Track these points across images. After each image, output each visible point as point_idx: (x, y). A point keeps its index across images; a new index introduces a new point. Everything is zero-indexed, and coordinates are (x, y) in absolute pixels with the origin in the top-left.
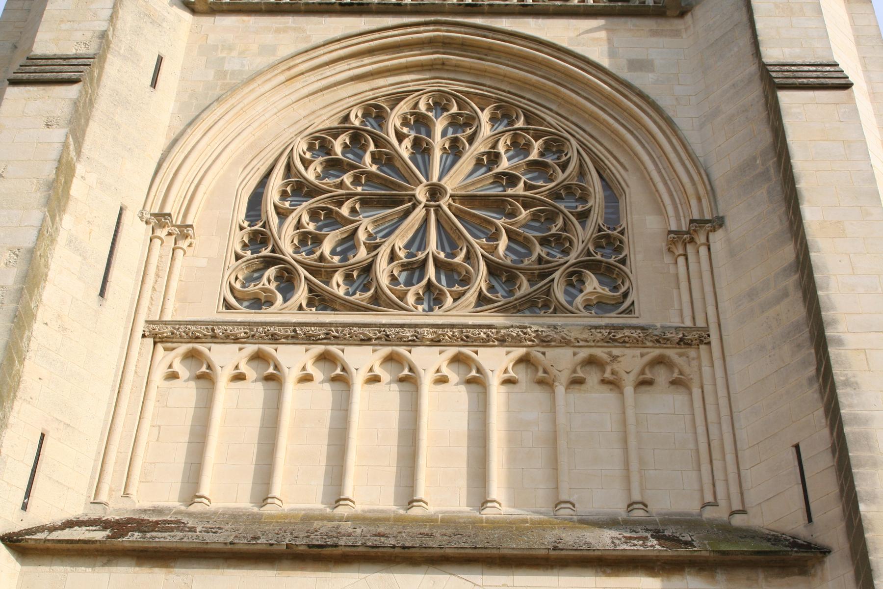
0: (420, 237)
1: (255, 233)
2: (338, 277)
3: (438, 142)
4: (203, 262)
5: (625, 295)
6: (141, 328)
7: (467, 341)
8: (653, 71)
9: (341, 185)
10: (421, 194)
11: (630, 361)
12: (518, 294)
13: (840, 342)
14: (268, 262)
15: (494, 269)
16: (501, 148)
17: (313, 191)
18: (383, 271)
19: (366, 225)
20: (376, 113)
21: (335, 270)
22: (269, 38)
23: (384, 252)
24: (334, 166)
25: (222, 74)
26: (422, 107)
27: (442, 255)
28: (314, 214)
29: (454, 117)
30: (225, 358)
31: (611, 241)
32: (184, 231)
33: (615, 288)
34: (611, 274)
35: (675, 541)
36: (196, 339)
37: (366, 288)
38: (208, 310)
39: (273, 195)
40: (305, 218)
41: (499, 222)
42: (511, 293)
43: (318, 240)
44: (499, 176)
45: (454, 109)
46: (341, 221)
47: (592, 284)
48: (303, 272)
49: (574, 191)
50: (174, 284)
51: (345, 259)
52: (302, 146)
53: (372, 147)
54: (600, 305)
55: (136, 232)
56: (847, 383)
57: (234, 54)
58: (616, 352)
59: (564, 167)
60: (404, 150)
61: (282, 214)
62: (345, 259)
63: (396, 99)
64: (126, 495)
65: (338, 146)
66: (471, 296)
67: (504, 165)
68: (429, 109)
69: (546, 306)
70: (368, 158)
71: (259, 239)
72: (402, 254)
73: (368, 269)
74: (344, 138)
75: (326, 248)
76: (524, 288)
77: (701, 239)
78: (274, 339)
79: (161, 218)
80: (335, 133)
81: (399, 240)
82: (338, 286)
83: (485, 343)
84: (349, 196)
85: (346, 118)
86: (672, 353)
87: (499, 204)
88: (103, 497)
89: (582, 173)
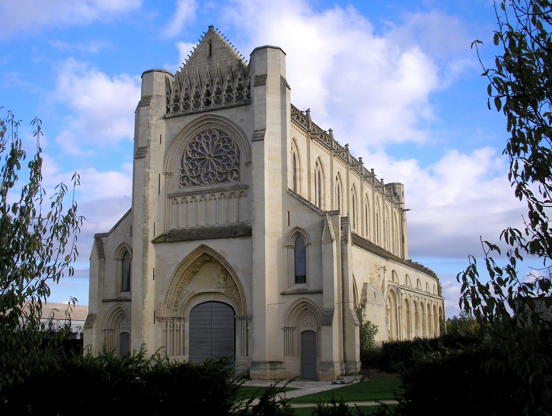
3: (210, 142)
7: (213, 192)
9: (195, 156)
11: (238, 192)
15: (219, 173)
31: (237, 164)
34: (237, 172)
38: (176, 190)
39: (185, 161)
47: (235, 175)
48: (190, 178)
49: (231, 152)
52: (188, 148)
54: (236, 179)
55: (163, 177)
70: (199, 149)
71: (183, 171)
76: (224, 176)
80: (193, 143)
82: (196, 181)
83: (216, 192)
86: (244, 190)
87: (220, 157)
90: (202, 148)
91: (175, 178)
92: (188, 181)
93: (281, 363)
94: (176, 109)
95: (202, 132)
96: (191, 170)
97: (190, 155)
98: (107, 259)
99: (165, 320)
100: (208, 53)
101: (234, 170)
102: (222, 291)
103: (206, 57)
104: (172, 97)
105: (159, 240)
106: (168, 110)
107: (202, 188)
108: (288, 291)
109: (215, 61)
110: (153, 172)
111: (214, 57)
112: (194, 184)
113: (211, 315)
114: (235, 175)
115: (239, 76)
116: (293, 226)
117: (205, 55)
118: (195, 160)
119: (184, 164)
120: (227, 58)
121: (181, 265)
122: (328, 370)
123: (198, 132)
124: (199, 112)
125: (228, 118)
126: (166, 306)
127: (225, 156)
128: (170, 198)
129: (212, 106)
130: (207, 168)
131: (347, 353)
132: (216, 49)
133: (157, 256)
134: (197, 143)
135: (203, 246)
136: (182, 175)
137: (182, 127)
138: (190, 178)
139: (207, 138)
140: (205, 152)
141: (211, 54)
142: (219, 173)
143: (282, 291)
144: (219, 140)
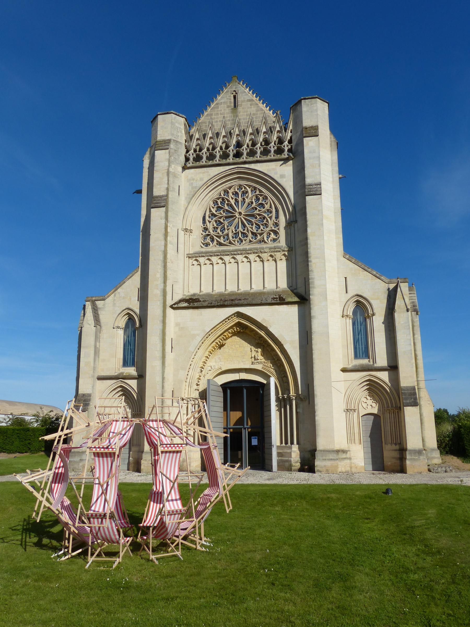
0: (237, 227)
1: (204, 228)
2: (222, 238)
3: (240, 199)
4: (195, 237)
5: (279, 238)
6: (186, 256)
8: (285, 178)
9: (221, 214)
10: (237, 215)
12: (258, 239)
13: (311, 261)
14: (208, 235)
16: (253, 201)
17: (215, 216)
18: (231, 235)
19: (226, 223)
20: (226, 192)
21: (221, 236)
22: (201, 175)
23: (230, 231)
24: (219, 208)
25: (193, 188)
26: (236, 190)
27: (242, 231)
28: (216, 221)
29: (243, 191)
30: (202, 260)
32: (191, 231)
33: (276, 236)
35: (158, 460)
36: (196, 257)
37: (228, 240)
38: (197, 249)
39: (207, 218)
40: (214, 223)
41: (253, 220)
42: (256, 239)
43: (217, 228)
44: (253, 208)
45: (243, 189)
46: (222, 223)
48: (215, 237)
50: (190, 244)
51: (223, 233)
52: (212, 204)
53: (226, 202)
55: (182, 233)
56: (311, 271)
57: (195, 181)
58: (275, 253)
59: (267, 204)
60: (233, 202)
61: (210, 222)
62: (223, 233)
63: (230, 188)
64: (189, 292)
65: (219, 201)
66: (248, 240)
67: (254, 205)
68: (238, 190)
69: (263, 241)
70: (226, 205)
71: (206, 229)
72: (234, 231)
73: (228, 235)
74: (221, 200)
75: (219, 231)
76: (259, 237)
77: (293, 225)
78: (211, 256)
79: (186, 230)
80: (218, 199)
81: (232, 228)
82: (222, 240)
84: (222, 216)
85: (220, 195)
87: (253, 216)
88: (185, 294)
89: (271, 206)
90: (231, 206)
91: (195, 237)
92: (212, 240)
93: (344, 452)
94: (198, 158)
95: (230, 188)
96: (215, 229)
97: (214, 211)
98: (104, 328)
99: (185, 401)
100: (233, 105)
101: (272, 231)
102: (259, 367)
103: (230, 108)
104: (194, 145)
105: (176, 306)
106: (187, 159)
107: (232, 248)
108: (350, 366)
109: (241, 114)
110: (171, 226)
111: (240, 109)
112: (220, 244)
113: (161, 428)
114: (273, 236)
115: (278, 128)
116: (352, 292)
117: (228, 107)
118: (220, 218)
119: (207, 221)
120: (257, 111)
121: (208, 334)
122: (167, 534)
123: (225, 187)
124: (229, 164)
125: (266, 172)
126: (187, 384)
127: (259, 215)
128: (189, 257)
129: (244, 158)
130: (237, 227)
131: (426, 440)
132: (242, 102)
133: (177, 324)
134: (223, 199)
135: (239, 315)
136: (204, 234)
137: (206, 180)
138: (215, 237)
139: (236, 194)
140: (234, 210)
141: (235, 106)
142: (253, 233)
143: (342, 367)
144: (252, 197)
